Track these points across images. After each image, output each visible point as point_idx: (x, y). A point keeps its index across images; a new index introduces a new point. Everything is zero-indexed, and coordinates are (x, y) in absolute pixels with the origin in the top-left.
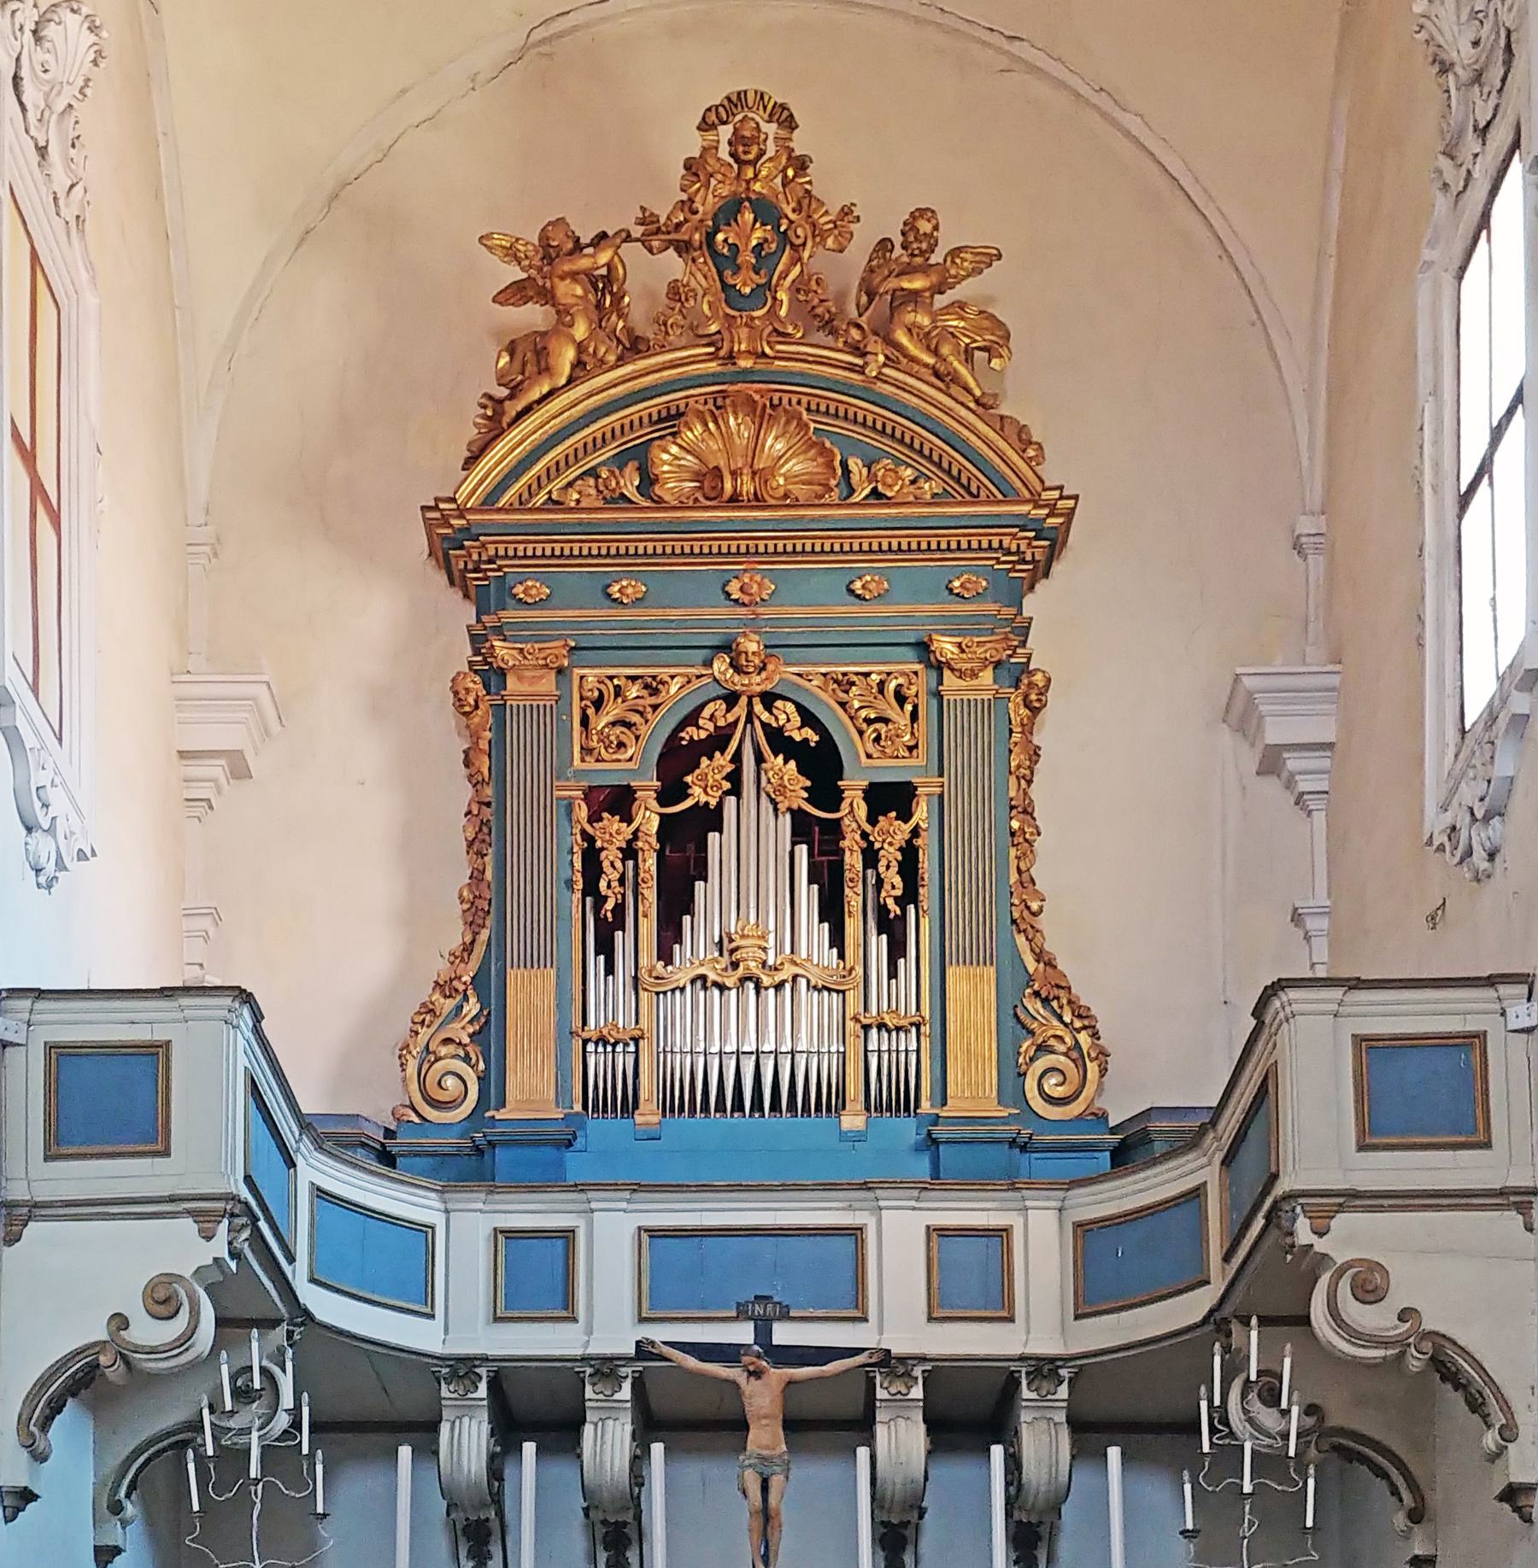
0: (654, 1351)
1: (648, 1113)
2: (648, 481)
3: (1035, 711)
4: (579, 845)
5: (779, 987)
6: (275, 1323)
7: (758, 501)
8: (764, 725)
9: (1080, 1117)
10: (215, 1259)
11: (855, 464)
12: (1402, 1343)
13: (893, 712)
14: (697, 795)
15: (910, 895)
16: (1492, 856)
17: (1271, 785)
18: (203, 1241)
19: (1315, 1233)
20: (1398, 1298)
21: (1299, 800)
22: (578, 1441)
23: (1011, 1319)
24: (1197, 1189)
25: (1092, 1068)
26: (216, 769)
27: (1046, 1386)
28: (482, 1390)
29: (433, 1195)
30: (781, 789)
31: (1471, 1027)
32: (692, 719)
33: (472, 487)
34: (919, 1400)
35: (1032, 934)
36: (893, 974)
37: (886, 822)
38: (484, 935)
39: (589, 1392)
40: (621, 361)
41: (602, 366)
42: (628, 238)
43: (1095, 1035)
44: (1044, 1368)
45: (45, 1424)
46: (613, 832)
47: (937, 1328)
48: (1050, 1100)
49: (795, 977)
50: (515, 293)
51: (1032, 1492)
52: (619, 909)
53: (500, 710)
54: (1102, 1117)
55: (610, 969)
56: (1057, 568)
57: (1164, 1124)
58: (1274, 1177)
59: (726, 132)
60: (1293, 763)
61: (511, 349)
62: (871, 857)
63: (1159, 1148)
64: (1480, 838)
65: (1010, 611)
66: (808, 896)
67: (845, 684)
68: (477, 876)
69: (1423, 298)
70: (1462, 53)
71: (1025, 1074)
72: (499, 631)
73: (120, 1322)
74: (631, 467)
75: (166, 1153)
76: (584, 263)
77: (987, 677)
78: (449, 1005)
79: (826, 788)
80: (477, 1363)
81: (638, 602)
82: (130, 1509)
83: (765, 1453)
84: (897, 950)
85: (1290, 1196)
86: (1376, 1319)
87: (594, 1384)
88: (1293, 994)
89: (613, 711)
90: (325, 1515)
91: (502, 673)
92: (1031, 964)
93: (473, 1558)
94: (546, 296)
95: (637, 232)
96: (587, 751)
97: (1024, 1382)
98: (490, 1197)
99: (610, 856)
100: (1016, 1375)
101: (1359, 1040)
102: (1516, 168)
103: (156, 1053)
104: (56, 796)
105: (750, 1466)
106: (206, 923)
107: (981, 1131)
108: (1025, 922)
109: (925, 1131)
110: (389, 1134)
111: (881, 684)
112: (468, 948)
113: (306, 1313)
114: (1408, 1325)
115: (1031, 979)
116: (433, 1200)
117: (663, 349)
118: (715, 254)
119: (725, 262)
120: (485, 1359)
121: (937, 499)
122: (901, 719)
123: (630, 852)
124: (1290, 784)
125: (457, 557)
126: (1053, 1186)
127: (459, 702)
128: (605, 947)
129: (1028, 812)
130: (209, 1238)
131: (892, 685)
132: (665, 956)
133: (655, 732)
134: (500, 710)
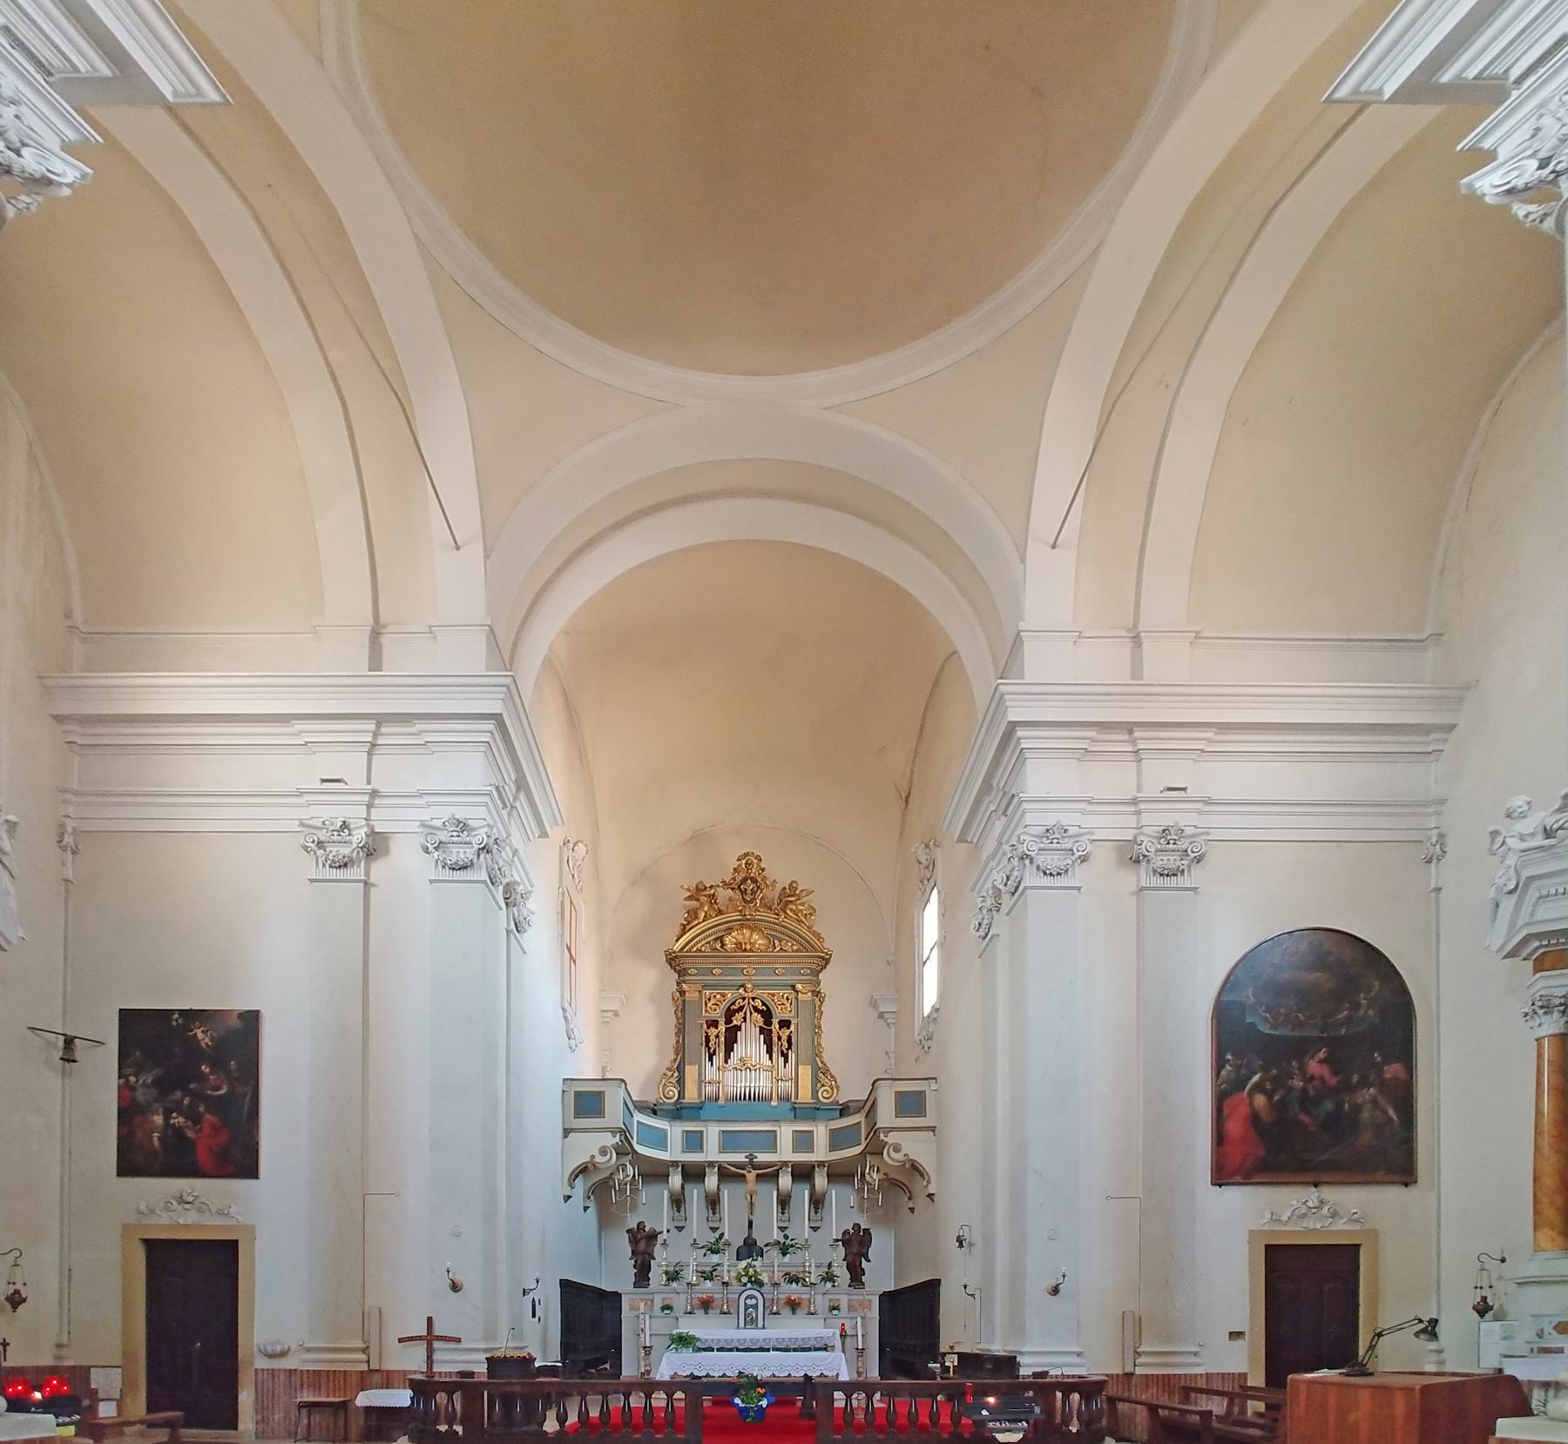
2: (723, 945)
3: (822, 1003)
4: (704, 1034)
5: (755, 1070)
6: (628, 1154)
7: (751, 951)
8: (753, 1006)
11: (776, 941)
13: (785, 1002)
14: (735, 1022)
15: (790, 1047)
16: (929, 1048)
17: (882, 1020)
20: (904, 1152)
21: (888, 1024)
22: (704, 1181)
25: (835, 1090)
26: (611, 1014)
30: (757, 1021)
31: (922, 1089)
32: (734, 1003)
33: (677, 947)
35: (821, 1057)
36: (785, 1067)
37: (784, 1030)
38: (679, 1057)
39: (707, 1169)
40: (716, 916)
41: (711, 917)
42: (718, 886)
43: (836, 1082)
44: (821, 1164)
45: (574, 1180)
46: (713, 1031)
48: (824, 1098)
49: (760, 1068)
50: (690, 898)
52: (714, 1051)
53: (684, 1001)
55: (712, 1065)
56: (828, 966)
57: (853, 1104)
58: (876, 1124)
59: (744, 861)
60: (886, 1016)
61: (688, 912)
62: (779, 1038)
63: (852, 1111)
64: (926, 1044)
65: (815, 978)
66: (764, 1048)
67: (773, 995)
68: (678, 1042)
69: (916, 914)
70: (924, 861)
72: (684, 982)
73: (593, 1157)
74: (719, 941)
75: (604, 1117)
76: (707, 893)
77: (810, 994)
78: (670, 1073)
79: (768, 1022)
81: (719, 975)
82: (592, 1198)
84: (786, 1061)
85: (879, 1128)
88: (881, 1082)
89: (713, 1001)
90: (863, 1349)
91: (685, 992)
92: (820, 1065)
94: (698, 900)
95: (721, 885)
96: (706, 1011)
99: (712, 1038)
101: (896, 1092)
102: (935, 890)
103: (600, 1095)
104: (575, 1030)
106: (608, 1052)
107: (807, 1106)
108: (817, 1054)
110: (655, 1105)
111: (783, 996)
112: (675, 1060)
113: (636, 1152)
115: (820, 1069)
116: (667, 1123)
117: (727, 913)
118: (741, 891)
119: (744, 892)
121: (796, 951)
122: (788, 1005)
123: (717, 1036)
124: (886, 1021)
125: (701, 1082)
126: (824, 1120)
127: (673, 999)
128: (711, 1059)
129: (820, 1027)
131: (785, 996)
132: (726, 1062)
133: (724, 1006)
134: (684, 1001)
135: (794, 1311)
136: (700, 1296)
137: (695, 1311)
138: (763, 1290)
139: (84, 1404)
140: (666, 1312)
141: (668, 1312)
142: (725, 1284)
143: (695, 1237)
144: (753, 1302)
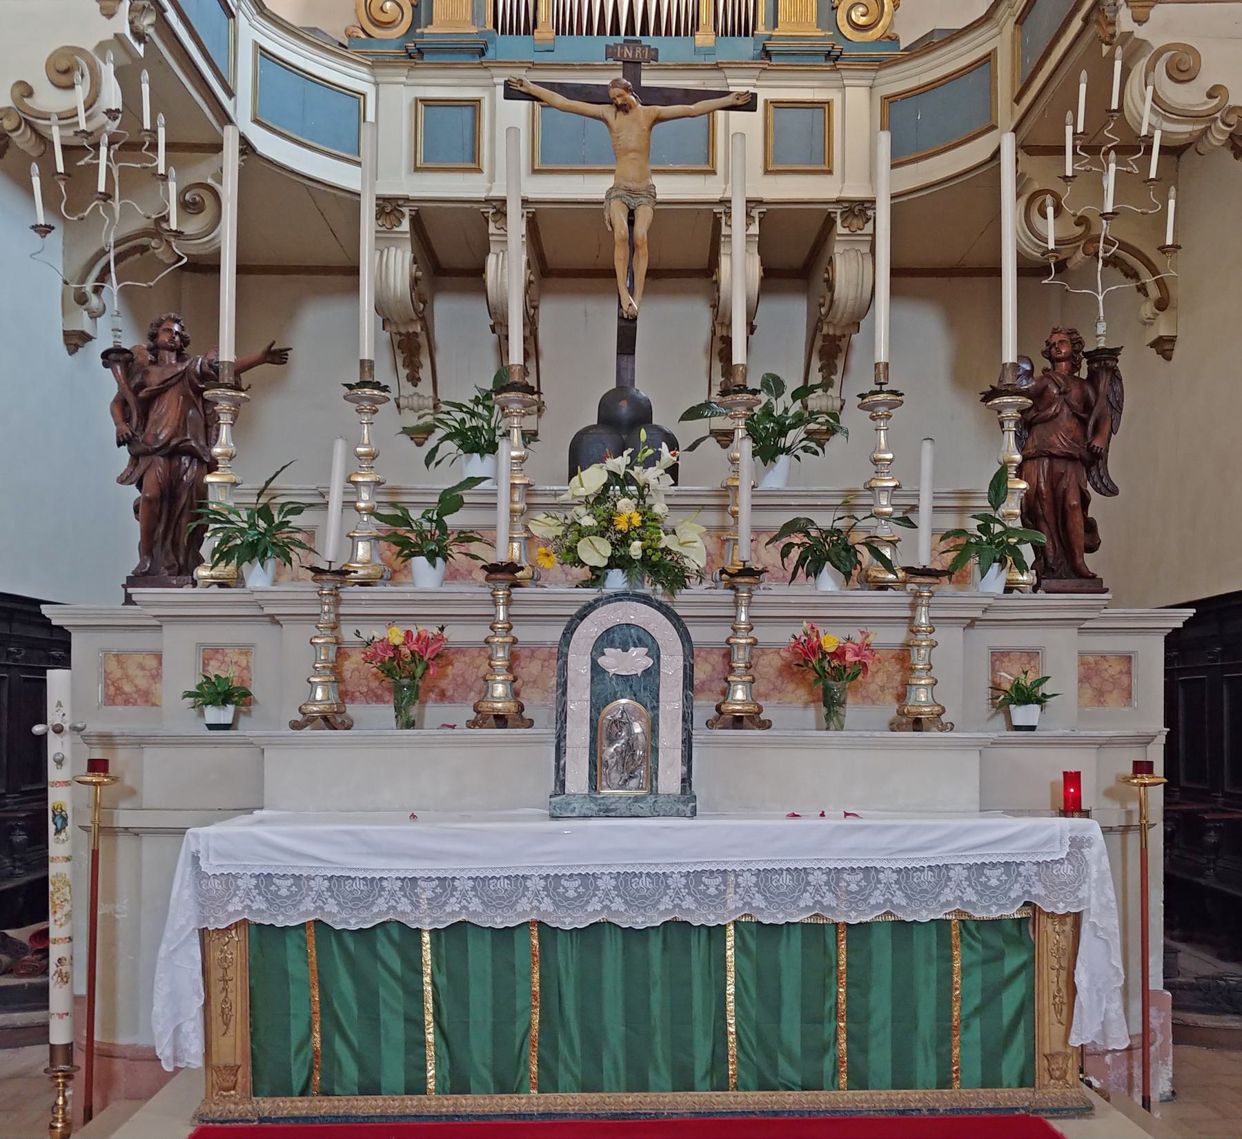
0: (522, 89)
1: (545, 30)
9: (878, 40)
10: (116, 35)
12: (1209, 117)
18: (104, 18)
19: (1135, 21)
20: (1206, 80)
23: (830, 172)
24: (989, 54)
27: (856, 223)
28: (406, 225)
29: (365, 69)
34: (755, 235)
47: (771, 179)
51: (841, 307)
54: (895, 40)
71: (837, 8)
73: (25, 90)
80: (400, 202)
83: (631, 185)
86: (1189, 96)
87: (495, 222)
93: (408, 366)
97: (839, 221)
98: (411, 73)
100: (833, 215)
105: (617, 197)
109: (761, 47)
114: (1216, 101)
116: (364, 73)
120: (407, 199)
130: (110, 15)
135: (831, 705)
136: (375, 632)
137: (352, 710)
138: (687, 599)
139: (534, 672)
140: (214, 714)
141: (224, 715)
142: (504, 572)
143: (366, 354)
144: (635, 660)
